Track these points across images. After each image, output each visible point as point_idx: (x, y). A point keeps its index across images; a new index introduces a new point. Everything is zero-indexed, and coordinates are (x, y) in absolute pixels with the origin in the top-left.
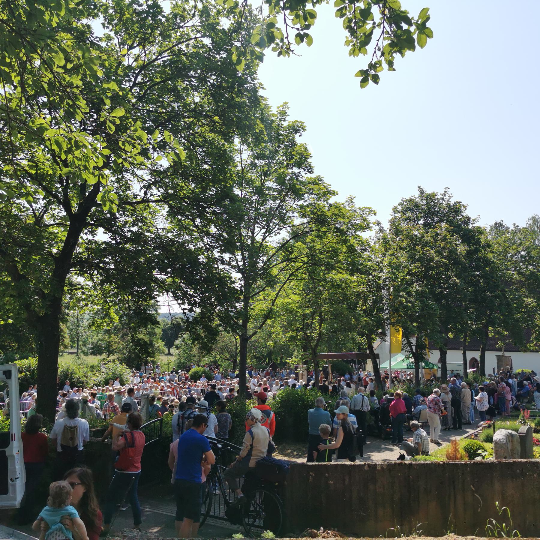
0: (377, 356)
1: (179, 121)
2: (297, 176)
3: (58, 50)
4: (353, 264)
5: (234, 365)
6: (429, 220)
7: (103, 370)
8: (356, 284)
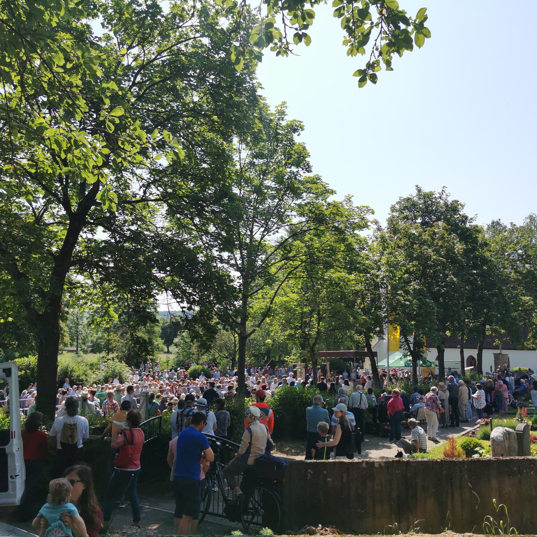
0: (375, 354)
1: (178, 121)
2: (295, 175)
3: (58, 49)
4: (351, 262)
5: (233, 363)
6: (427, 219)
7: (103, 368)
8: (354, 282)
